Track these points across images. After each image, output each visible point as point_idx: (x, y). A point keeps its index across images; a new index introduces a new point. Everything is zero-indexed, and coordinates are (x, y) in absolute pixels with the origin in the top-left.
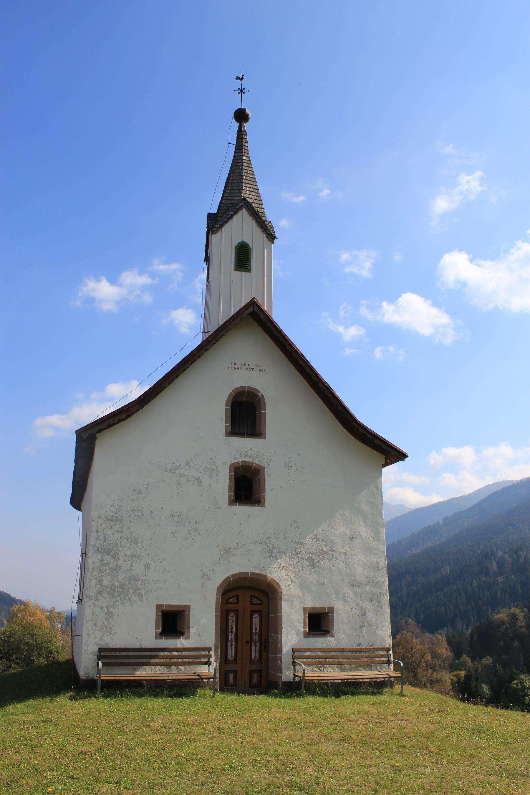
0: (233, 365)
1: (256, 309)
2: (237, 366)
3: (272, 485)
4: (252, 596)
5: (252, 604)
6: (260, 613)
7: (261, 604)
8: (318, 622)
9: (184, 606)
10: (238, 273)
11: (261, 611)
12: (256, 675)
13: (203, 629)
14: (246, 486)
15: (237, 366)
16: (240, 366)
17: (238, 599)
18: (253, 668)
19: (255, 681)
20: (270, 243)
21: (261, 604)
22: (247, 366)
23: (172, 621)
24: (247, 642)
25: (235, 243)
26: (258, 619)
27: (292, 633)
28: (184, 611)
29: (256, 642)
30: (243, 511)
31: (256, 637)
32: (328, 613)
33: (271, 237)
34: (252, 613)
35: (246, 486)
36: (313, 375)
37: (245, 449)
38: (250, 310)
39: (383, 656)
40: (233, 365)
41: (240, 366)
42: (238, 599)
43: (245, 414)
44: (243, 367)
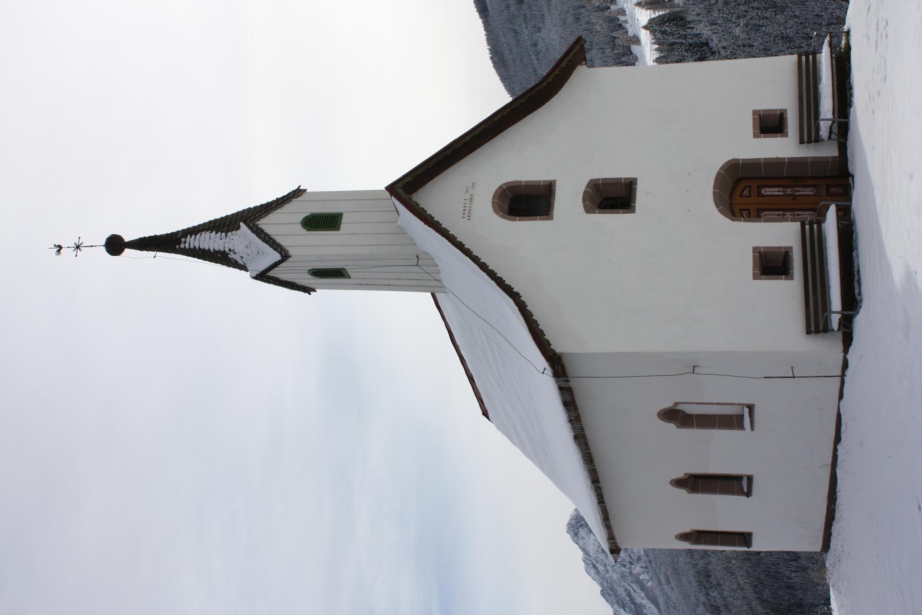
0: (466, 216)
1: (400, 185)
2: (467, 212)
3: (614, 169)
4: (741, 196)
5: (750, 196)
6: (760, 188)
7: (750, 187)
8: (769, 124)
9: (754, 252)
10: (343, 226)
11: (758, 187)
12: (832, 190)
13: (782, 234)
14: (612, 197)
15: (467, 212)
16: (467, 209)
17: (745, 210)
18: (824, 192)
19: (839, 190)
20: (304, 194)
21: (750, 187)
22: (468, 202)
23: (771, 264)
24: (794, 199)
25: (304, 231)
26: (767, 189)
27: (783, 148)
28: (760, 253)
29: (795, 191)
30: (641, 198)
31: (789, 191)
32: (760, 116)
33: (298, 193)
34: (760, 195)
35: (612, 197)
36: (483, 127)
37: (568, 199)
38: (401, 192)
39: (807, 59)
40: (466, 216)
41: (467, 209)
42: (745, 210)
43: (526, 201)
44: (468, 205)
